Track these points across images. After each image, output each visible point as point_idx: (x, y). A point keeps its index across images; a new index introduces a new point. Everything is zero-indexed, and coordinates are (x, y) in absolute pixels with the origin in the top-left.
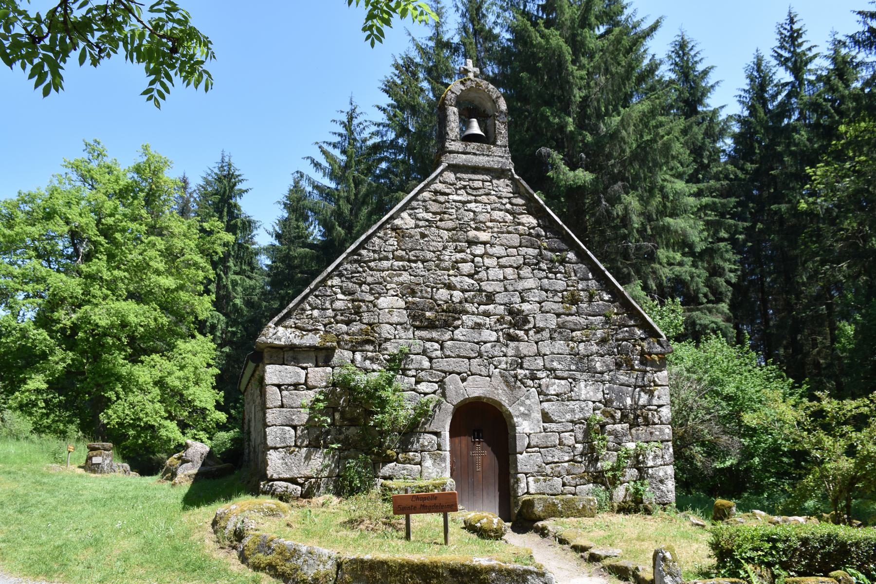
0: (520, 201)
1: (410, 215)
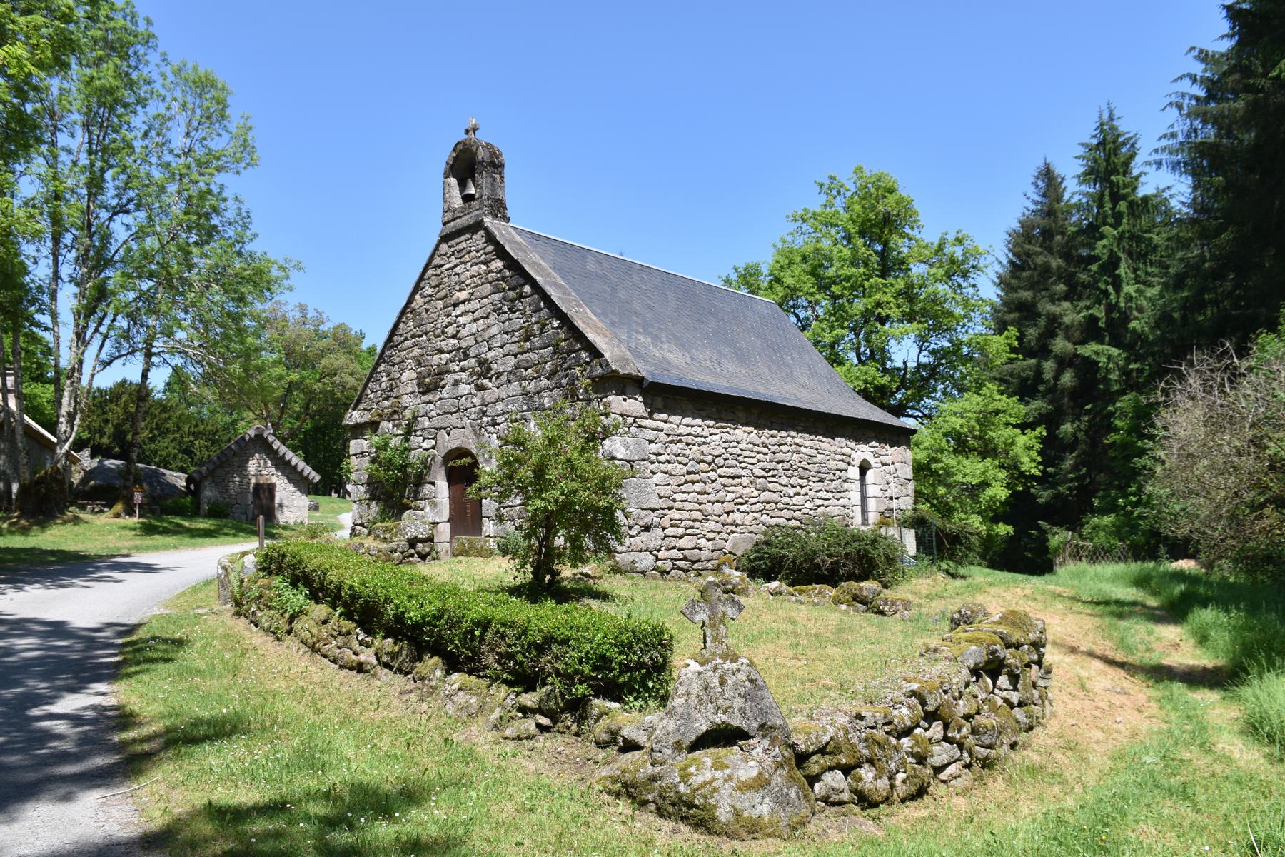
0: (491, 248)
1: (1268, 488)
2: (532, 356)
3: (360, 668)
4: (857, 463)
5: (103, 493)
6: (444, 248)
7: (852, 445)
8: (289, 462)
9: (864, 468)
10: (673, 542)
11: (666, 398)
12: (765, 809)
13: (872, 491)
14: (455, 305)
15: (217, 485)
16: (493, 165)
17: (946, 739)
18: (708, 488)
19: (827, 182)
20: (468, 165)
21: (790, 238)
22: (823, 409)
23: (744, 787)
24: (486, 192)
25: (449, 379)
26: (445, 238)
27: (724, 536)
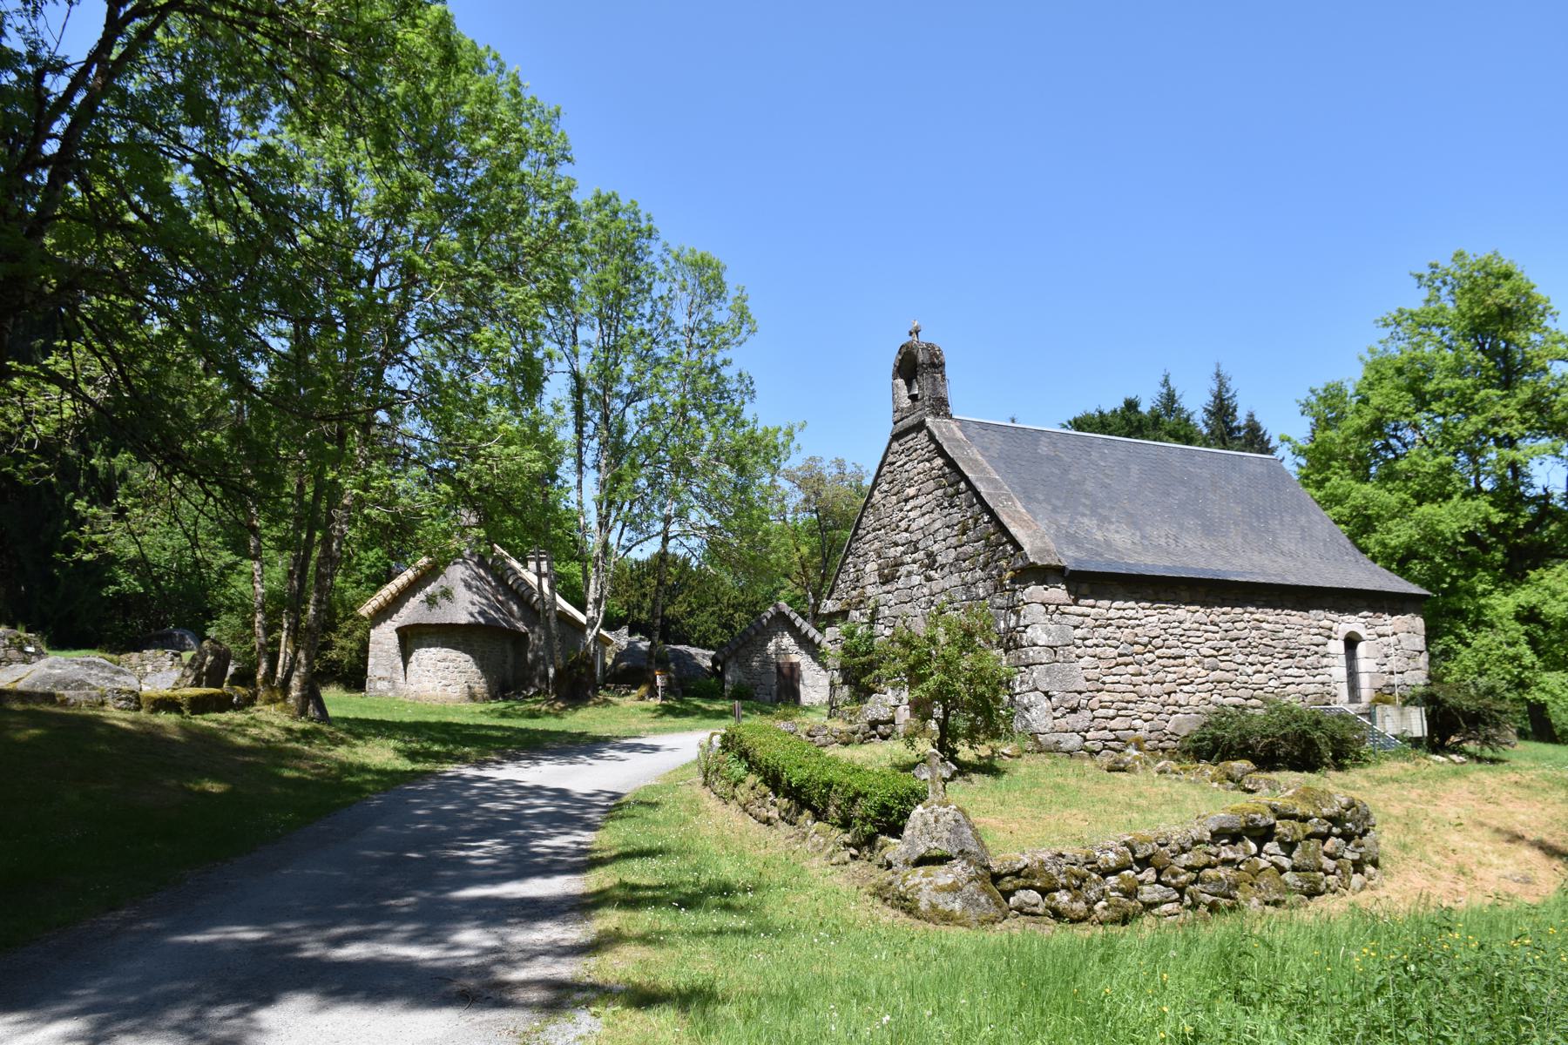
0: (933, 446)
2: (968, 549)
3: (768, 822)
4: (1342, 635)
5: (630, 675)
6: (895, 446)
7: (1335, 616)
8: (812, 640)
9: (1351, 642)
10: (1104, 723)
11: (1089, 584)
12: (957, 906)
13: (1364, 665)
14: (906, 501)
15: (740, 666)
16: (933, 365)
17: (1158, 881)
18: (1143, 670)
19: (1427, 272)
20: (915, 366)
21: (1380, 348)
22: (1292, 580)
23: (942, 889)
24: (927, 393)
25: (903, 570)
26: (896, 437)
27: (1164, 716)
